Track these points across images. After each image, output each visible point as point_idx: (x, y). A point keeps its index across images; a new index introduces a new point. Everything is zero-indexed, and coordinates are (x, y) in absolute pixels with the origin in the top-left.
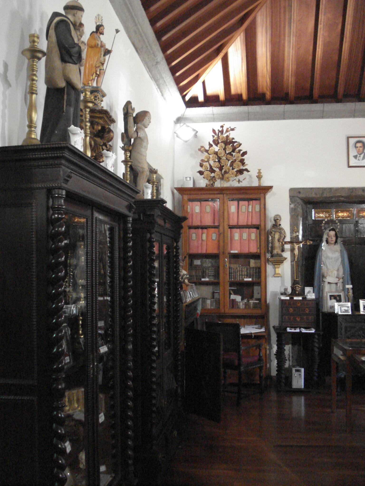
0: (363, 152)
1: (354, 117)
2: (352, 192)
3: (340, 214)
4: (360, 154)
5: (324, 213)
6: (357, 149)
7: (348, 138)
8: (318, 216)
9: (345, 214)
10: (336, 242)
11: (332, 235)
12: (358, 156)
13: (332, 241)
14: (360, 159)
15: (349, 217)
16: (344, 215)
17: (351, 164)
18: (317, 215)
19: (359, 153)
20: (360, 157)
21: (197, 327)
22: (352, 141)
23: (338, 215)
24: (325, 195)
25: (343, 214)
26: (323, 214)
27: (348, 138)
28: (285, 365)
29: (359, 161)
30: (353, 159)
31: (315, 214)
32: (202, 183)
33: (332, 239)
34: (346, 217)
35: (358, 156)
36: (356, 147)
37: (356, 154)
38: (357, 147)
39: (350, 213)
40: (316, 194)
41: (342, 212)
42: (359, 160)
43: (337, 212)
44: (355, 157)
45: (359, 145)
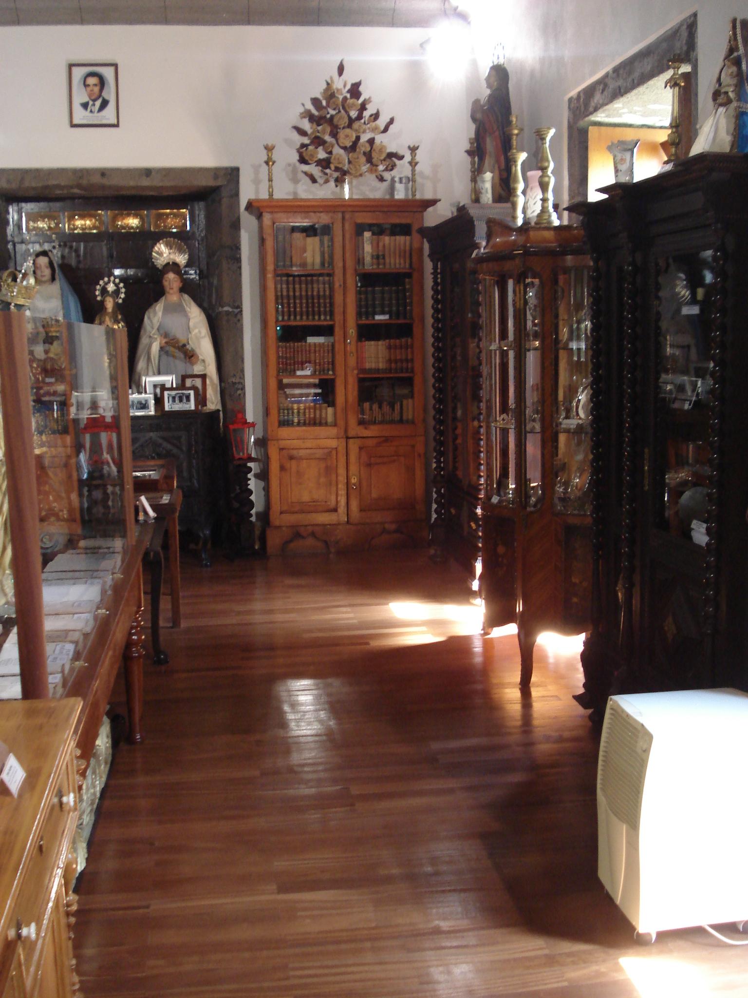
0: (100, 96)
1: (82, 22)
2: (22, 179)
3: (79, 223)
4: (94, 100)
5: (46, 220)
6: (89, 89)
7: (71, 66)
8: (34, 227)
9: (88, 222)
10: (53, 279)
11: (43, 265)
12: (91, 103)
13: (44, 276)
14: (93, 110)
15: (94, 227)
16: (85, 224)
17: (76, 121)
18: (31, 224)
19: (93, 98)
20: (94, 105)
21: (390, 240)
22: (79, 73)
23: (74, 225)
24: (27, 184)
25: (83, 222)
26: (44, 221)
27: (71, 66)
28: (669, 135)
29: (91, 115)
30: (81, 109)
31: (27, 222)
32: (385, 166)
33: (42, 272)
34: (90, 229)
35: (91, 103)
36: (86, 85)
37: (86, 99)
38: (89, 85)
39: (96, 220)
40: (8, 181)
41: (82, 217)
42: (91, 111)
43: (71, 218)
44: (85, 106)
45: (92, 81)
